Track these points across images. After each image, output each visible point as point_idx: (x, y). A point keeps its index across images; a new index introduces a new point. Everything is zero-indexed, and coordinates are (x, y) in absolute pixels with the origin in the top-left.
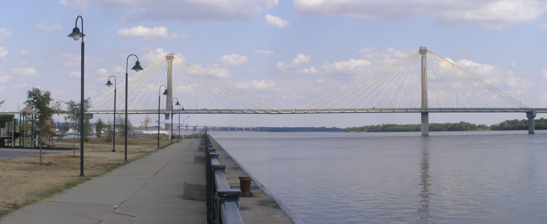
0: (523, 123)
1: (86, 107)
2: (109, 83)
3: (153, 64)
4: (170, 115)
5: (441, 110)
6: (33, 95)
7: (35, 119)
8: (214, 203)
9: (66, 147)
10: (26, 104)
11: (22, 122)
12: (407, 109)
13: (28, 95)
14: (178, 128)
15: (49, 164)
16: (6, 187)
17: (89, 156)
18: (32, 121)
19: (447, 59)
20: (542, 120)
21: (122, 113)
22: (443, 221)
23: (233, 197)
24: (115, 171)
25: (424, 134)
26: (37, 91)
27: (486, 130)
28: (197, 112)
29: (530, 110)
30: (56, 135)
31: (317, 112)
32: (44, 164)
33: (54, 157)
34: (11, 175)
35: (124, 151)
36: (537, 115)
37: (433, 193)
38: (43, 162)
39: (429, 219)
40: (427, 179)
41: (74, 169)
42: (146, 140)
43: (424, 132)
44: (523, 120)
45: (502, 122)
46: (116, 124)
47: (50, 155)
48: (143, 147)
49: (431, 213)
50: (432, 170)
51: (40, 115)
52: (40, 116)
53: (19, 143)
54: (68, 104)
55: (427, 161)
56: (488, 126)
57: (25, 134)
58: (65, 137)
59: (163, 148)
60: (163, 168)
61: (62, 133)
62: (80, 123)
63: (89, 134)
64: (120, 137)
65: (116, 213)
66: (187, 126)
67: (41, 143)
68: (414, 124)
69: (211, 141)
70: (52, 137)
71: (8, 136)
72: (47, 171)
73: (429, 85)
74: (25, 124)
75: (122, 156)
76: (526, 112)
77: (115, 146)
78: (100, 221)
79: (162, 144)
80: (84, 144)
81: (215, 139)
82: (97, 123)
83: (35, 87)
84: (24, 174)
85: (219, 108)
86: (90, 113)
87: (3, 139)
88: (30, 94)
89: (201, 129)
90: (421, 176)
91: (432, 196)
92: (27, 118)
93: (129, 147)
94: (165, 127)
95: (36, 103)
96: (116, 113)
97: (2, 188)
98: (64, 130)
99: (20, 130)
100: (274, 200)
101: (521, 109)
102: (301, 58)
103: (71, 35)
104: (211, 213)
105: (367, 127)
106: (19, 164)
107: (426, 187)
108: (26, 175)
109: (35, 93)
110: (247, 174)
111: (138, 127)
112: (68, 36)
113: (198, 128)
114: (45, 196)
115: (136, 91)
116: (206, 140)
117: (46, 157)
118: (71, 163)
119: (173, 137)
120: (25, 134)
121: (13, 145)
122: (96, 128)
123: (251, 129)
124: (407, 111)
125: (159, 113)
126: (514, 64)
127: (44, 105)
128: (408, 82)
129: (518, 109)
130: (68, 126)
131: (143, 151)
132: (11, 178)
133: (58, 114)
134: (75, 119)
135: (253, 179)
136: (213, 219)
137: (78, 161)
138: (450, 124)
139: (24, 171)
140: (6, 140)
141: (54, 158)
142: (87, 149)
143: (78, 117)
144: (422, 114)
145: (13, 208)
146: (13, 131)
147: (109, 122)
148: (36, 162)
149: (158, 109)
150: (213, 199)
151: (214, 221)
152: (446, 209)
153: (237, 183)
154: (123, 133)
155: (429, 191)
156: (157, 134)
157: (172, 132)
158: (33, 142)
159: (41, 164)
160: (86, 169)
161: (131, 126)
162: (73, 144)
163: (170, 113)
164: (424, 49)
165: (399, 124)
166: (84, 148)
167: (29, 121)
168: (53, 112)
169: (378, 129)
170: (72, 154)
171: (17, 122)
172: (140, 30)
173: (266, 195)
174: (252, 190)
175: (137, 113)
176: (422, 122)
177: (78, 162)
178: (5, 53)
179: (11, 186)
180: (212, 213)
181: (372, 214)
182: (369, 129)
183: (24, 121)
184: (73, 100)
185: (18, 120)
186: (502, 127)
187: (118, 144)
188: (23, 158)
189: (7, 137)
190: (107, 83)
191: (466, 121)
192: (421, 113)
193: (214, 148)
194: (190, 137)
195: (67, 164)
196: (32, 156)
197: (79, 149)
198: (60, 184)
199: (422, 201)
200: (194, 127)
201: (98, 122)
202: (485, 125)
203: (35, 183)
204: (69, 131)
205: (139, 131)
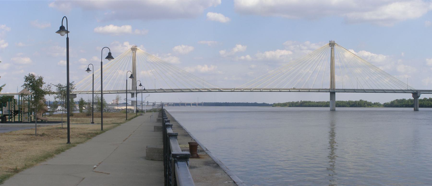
0: (410, 101)
1: (71, 88)
2: (88, 70)
3: (122, 54)
4: (135, 94)
5: (345, 91)
6: (29, 80)
7: (31, 99)
9: (56, 121)
10: (23, 86)
11: (20, 101)
12: (319, 89)
13: (25, 79)
14: (141, 104)
15: (43, 135)
17: (74, 128)
18: (29, 100)
19: (350, 50)
20: (425, 100)
21: (99, 93)
22: (345, 178)
23: (184, 158)
24: (94, 139)
25: (332, 109)
26: (32, 76)
27: (379, 107)
28: (155, 91)
29: (415, 91)
30: (47, 112)
32: (39, 135)
33: (47, 129)
34: (12, 145)
35: (101, 123)
36: (421, 95)
37: (338, 156)
38: (38, 133)
39: (335, 176)
40: (333, 145)
41: (62, 138)
42: (117, 114)
44: (410, 99)
45: (392, 101)
46: (95, 101)
47: (43, 128)
48: (115, 120)
49: (336, 171)
50: (337, 138)
51: (35, 95)
52: (34, 96)
53: (18, 119)
54: (57, 86)
55: (334, 130)
56: (381, 104)
57: (23, 111)
58: (55, 113)
59: (130, 120)
60: (130, 136)
61: (53, 110)
62: (67, 102)
63: (74, 110)
64: (97, 112)
65: (95, 172)
66: (148, 103)
67: (36, 118)
68: (324, 101)
69: (167, 114)
70: (45, 113)
71: (9, 113)
72: (42, 141)
73: (336, 71)
74: (23, 104)
75: (99, 127)
76: (412, 93)
77: (94, 119)
78: (83, 178)
79: (129, 116)
80: (70, 118)
81: (169, 113)
82: (80, 101)
83: (31, 73)
84: (22, 144)
85: (172, 88)
86: (74, 93)
88: (26, 79)
89: (159, 105)
90: (329, 142)
92: (25, 98)
93: (104, 119)
94: (132, 104)
95: (31, 86)
96: (94, 93)
97: (4, 156)
98: (54, 107)
99: (19, 108)
100: (214, 161)
101: (408, 90)
102: (239, 47)
103: (58, 32)
104: (167, 170)
105: (289, 103)
106: (18, 136)
107: (333, 151)
108: (25, 145)
109: (31, 78)
110: (194, 140)
111: (111, 103)
112: (56, 32)
113: (156, 104)
115: (109, 76)
116: (162, 113)
117: (40, 129)
118: (60, 133)
119: (137, 111)
120: (23, 111)
121: (13, 121)
122: (79, 106)
123: (197, 104)
124: (319, 91)
125: (127, 93)
126: (403, 54)
127: (38, 88)
128: (320, 68)
129: (406, 90)
130: (57, 104)
131: (115, 122)
132: (12, 147)
133: (49, 95)
134: (63, 98)
135: (199, 144)
136: (169, 176)
137: (65, 132)
138: (352, 102)
139: (23, 141)
140: (7, 117)
141: (47, 130)
142: (72, 122)
143: (65, 97)
144: (330, 93)
145: (14, 172)
146: (13, 109)
147: (89, 100)
148: (32, 134)
149: (125, 89)
150: (169, 159)
151: (170, 177)
152: (348, 169)
153: (187, 147)
154: (100, 109)
155: (335, 154)
156: (125, 109)
157: (137, 107)
158: (30, 118)
159: (36, 135)
160: (72, 138)
161: (106, 103)
162: (61, 118)
163: (135, 93)
164: (332, 42)
165: (313, 101)
166: (70, 121)
167: (26, 100)
168: (45, 93)
169: (297, 105)
170: (61, 126)
171: (16, 101)
172: (111, 28)
173: (210, 157)
174: (199, 153)
175: (110, 93)
177: (66, 132)
178: (5, 45)
179: (12, 154)
180: (168, 171)
181: (291, 171)
182: (290, 104)
183: (22, 100)
184: (60, 83)
185: (17, 100)
186: (392, 105)
187: (96, 117)
188: (21, 131)
189: (8, 114)
190: (87, 70)
191: (364, 99)
192: (330, 93)
193: (168, 119)
194: (150, 111)
195: (57, 134)
196: (29, 129)
197: (66, 122)
198: (52, 150)
199: (330, 162)
200: (154, 103)
201: (81, 100)
202: (379, 103)
203: (32, 150)
204: (58, 108)
205: (111, 107)
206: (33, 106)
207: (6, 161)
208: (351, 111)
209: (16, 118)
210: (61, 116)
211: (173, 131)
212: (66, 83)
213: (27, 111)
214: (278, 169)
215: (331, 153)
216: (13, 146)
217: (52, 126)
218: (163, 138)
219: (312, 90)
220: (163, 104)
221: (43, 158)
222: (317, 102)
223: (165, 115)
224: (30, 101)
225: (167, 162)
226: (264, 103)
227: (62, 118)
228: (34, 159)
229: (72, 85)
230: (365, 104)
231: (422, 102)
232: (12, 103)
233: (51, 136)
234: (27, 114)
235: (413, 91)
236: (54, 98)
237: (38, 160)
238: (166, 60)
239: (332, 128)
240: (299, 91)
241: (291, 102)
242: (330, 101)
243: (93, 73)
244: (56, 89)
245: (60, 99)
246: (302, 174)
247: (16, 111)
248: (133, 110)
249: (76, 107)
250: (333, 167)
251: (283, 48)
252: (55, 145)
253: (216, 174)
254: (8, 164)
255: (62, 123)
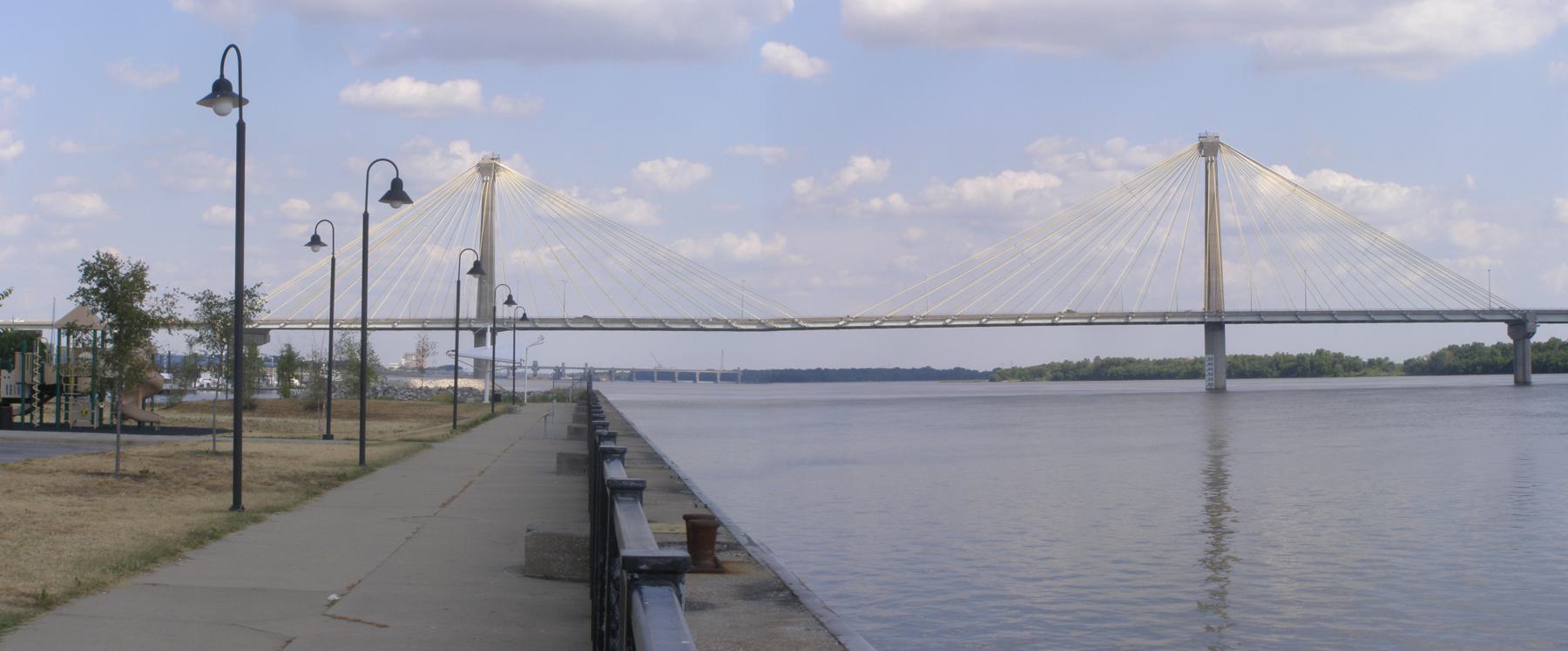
0: (1499, 353)
1: (252, 309)
2: (315, 241)
3: (442, 186)
4: (489, 334)
5: (1260, 318)
6: (95, 275)
7: (102, 345)
8: (612, 589)
9: (192, 426)
10: (75, 298)
11: (63, 352)
12: (1164, 315)
13: (83, 273)
14: (511, 371)
15: (142, 476)
16: (15, 544)
17: (256, 453)
18: (94, 350)
19: (1276, 168)
21: (352, 326)
22: (1267, 638)
23: (666, 573)
24: (331, 496)
25: (1213, 387)
27: (1389, 375)
28: (565, 325)
29: (1517, 316)
30: (161, 392)
31: (910, 324)
32: (127, 475)
33: (157, 456)
35: (358, 437)
36: (1538, 329)
37: (1239, 557)
39: (1227, 631)
41: (213, 489)
43: (1213, 382)
44: (1499, 343)
45: (1436, 351)
46: (336, 358)
47: (144, 451)
49: (1233, 615)
50: (1235, 491)
51: (116, 331)
52: (115, 334)
53: (54, 415)
54: (198, 300)
55: (1221, 464)
56: (1396, 362)
57: (72, 389)
58: (188, 398)
59: (466, 428)
61: (181, 385)
62: (232, 357)
66: (535, 367)
67: (119, 413)
69: (605, 408)
71: (23, 394)
72: (139, 497)
73: (1227, 244)
74: (73, 360)
75: (352, 451)
76: (1506, 321)
78: (288, 640)
79: (466, 416)
80: (245, 418)
81: (615, 405)
83: (103, 251)
84: (68, 506)
85: (628, 316)
87: (8, 401)
88: (87, 270)
89: (577, 374)
90: (1205, 506)
91: (1235, 566)
92: (79, 340)
93: (371, 425)
94: (475, 369)
95: (104, 297)
96: (336, 329)
99: (59, 377)
100: (783, 583)
101: (1493, 312)
102: (864, 165)
103: (207, 101)
104: (602, 617)
105: (1052, 366)
106: (54, 475)
108: (75, 509)
109: (103, 269)
110: (706, 506)
111: (396, 367)
113: (567, 371)
114: (130, 569)
118: (205, 473)
119: (496, 397)
120: (72, 389)
121: (36, 421)
122: (278, 372)
123: (718, 377)
124: (1163, 319)
125: (457, 329)
127: (130, 304)
129: (1484, 312)
130: (195, 365)
132: (30, 517)
133: (169, 330)
135: (723, 521)
138: (1287, 358)
139: (69, 496)
140: (16, 406)
142: (251, 432)
145: (35, 606)
146: (37, 379)
147: (315, 354)
148: (103, 471)
149: (452, 315)
151: (612, 641)
152: (1276, 603)
153: (677, 531)
154: (355, 384)
155: (1227, 550)
156: (450, 387)
158: (96, 412)
159: (119, 475)
160: (249, 490)
161: (379, 366)
162: (211, 417)
164: (1210, 141)
167: (85, 349)
168: (155, 323)
169: (1081, 374)
170: (209, 446)
171: (49, 352)
172: (405, 89)
174: (722, 553)
175: (394, 327)
176: (1206, 353)
177: (227, 469)
178: (14, 150)
179: (30, 540)
180: (605, 619)
182: (1056, 371)
183: (68, 349)
184: (211, 290)
185: (52, 345)
186: (1435, 366)
187: (341, 416)
188: (65, 458)
189: (20, 396)
190: (310, 240)
191: (1333, 347)
192: (1203, 326)
193: (611, 429)
194: (544, 398)
195: (196, 476)
196: (93, 454)
199: (1208, 580)
200: (557, 369)
202: (1387, 359)
203: (101, 531)
204: (201, 380)
206: (110, 371)
207: (6, 566)
208: (1283, 391)
209: (48, 413)
210: (213, 407)
211: (627, 473)
212: (233, 290)
213: (88, 386)
214: (1014, 612)
215: (1215, 549)
216: (34, 513)
217: (177, 445)
218: (590, 496)
219: (1136, 317)
220: (592, 373)
221: (143, 562)
222: (1158, 363)
223: (598, 415)
224: (99, 351)
225: (603, 585)
226: (958, 369)
227: (214, 418)
228: (109, 564)
229: (256, 296)
230: (1335, 363)
231: (1544, 354)
232: (34, 357)
233: (174, 480)
234: (89, 397)
235: (1511, 315)
236: (187, 343)
237: (122, 566)
238: (606, 210)
239: (1215, 457)
240: (1090, 321)
241: (1060, 364)
242: (1204, 355)
243: (333, 254)
244: (196, 310)
245: (208, 347)
246: (1107, 625)
247: (49, 385)
248: (479, 392)
249: (266, 378)
250: (1223, 599)
251: (1025, 163)
252: (188, 515)
253: (787, 628)
254: (16, 577)
255: (214, 437)
